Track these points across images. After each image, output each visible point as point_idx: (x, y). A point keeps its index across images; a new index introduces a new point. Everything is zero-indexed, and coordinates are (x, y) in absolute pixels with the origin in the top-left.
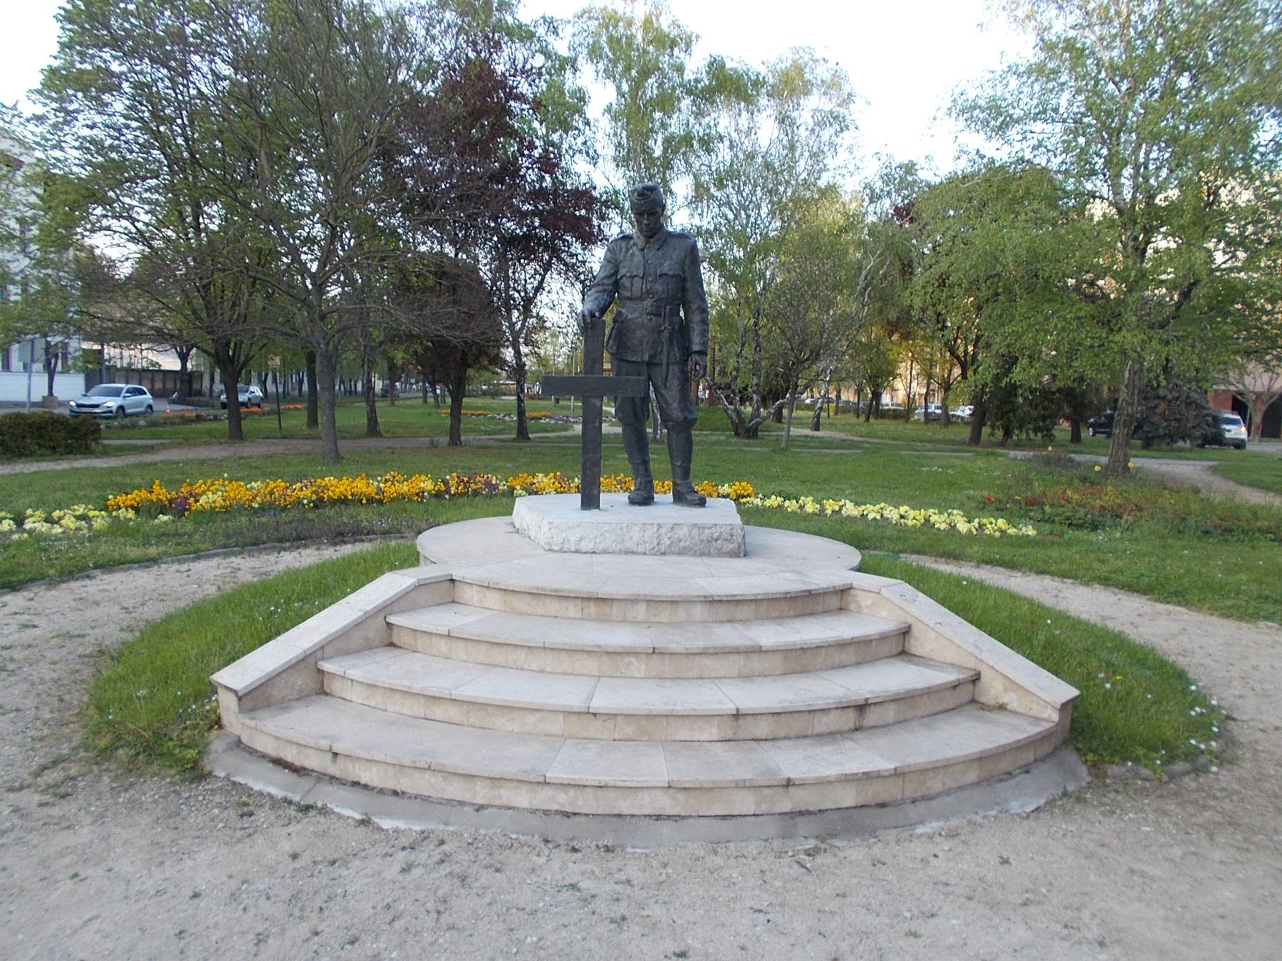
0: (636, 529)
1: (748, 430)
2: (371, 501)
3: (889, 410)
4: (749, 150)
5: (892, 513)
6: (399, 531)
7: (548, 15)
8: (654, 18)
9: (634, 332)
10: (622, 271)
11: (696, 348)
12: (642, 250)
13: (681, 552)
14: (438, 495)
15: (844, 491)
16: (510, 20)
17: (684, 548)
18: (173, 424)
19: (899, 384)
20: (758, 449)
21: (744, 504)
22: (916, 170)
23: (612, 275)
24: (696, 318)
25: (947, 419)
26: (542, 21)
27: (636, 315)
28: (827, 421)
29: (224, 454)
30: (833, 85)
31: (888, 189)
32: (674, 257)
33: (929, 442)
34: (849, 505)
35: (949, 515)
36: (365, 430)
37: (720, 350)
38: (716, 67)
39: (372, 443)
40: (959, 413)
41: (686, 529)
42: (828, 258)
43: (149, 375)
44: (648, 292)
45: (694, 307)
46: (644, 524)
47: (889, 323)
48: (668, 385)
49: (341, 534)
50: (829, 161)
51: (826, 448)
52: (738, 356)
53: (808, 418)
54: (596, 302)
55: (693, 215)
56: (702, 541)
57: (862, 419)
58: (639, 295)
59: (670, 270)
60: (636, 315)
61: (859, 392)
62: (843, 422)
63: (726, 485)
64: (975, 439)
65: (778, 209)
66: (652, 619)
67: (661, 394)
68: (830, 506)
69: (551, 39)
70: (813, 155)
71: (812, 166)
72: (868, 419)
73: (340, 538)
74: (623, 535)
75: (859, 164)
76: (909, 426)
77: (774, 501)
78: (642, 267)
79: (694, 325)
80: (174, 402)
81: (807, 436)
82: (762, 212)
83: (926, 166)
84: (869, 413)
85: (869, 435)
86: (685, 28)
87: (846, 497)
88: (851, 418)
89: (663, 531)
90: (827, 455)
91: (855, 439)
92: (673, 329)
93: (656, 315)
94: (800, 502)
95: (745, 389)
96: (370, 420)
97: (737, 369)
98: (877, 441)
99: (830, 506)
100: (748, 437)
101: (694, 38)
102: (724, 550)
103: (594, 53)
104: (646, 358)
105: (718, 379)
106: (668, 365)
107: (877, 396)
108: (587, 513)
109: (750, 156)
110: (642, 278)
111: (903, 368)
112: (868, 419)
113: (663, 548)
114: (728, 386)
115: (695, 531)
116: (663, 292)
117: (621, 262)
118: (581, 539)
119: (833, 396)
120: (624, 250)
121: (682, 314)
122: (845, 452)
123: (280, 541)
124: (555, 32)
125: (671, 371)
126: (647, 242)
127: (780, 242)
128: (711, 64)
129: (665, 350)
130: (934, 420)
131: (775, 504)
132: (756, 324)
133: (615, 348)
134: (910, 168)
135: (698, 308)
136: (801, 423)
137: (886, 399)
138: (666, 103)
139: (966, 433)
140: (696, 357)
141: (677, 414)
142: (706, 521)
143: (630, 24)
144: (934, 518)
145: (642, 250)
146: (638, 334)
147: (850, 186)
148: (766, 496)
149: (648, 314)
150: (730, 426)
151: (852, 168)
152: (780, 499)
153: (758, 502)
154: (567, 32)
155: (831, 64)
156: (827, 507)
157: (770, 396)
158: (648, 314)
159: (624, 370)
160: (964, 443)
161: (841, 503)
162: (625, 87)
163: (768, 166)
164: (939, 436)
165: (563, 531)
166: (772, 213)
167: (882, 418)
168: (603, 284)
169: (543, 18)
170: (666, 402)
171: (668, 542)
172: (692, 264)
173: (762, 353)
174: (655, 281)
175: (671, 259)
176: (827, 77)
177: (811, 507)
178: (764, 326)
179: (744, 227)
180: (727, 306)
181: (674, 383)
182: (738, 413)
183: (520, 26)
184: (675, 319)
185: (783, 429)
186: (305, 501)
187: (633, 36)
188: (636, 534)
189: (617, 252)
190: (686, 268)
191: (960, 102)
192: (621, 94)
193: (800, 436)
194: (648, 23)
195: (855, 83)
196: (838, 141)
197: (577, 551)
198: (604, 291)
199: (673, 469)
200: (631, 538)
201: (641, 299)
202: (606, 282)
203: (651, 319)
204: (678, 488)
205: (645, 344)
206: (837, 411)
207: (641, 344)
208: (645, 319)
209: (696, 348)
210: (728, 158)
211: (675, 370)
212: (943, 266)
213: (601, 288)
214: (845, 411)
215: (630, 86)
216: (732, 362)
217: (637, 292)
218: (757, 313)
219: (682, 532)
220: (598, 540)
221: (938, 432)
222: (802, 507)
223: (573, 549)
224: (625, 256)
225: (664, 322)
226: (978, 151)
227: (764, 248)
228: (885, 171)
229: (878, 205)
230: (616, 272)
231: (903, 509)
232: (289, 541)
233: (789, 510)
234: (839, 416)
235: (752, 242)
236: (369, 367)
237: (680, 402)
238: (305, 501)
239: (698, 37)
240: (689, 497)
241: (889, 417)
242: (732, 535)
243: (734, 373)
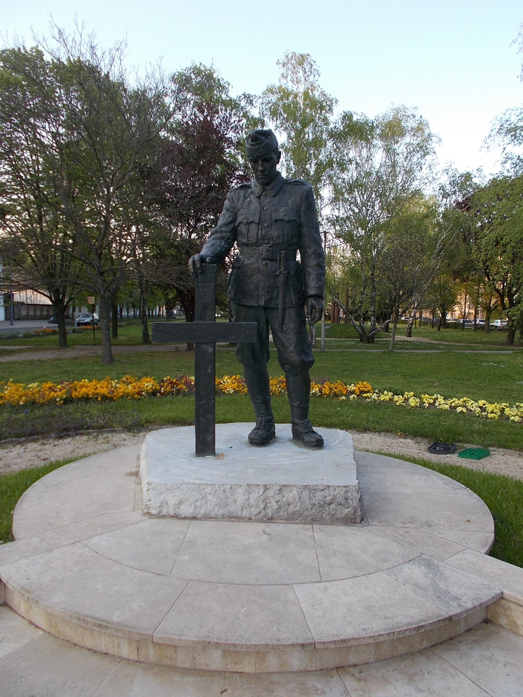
0: (241, 491)
1: (368, 338)
2: (105, 398)
3: (451, 323)
4: (368, 171)
5: (474, 406)
6: (111, 426)
7: (247, 92)
8: (310, 91)
9: (251, 276)
10: (240, 219)
11: (312, 292)
12: (259, 197)
13: (291, 518)
14: (154, 393)
15: (433, 383)
16: (224, 96)
17: (293, 513)
18: (38, 336)
19: (456, 308)
20: (374, 351)
21: (366, 398)
22: (472, 178)
23: (230, 223)
24: (312, 262)
25: (488, 329)
26: (243, 97)
27: (252, 260)
28: (415, 330)
29: (52, 356)
30: (419, 129)
31: (454, 190)
32: (290, 202)
33: (480, 343)
34: (441, 400)
35: (517, 407)
36: (141, 340)
37: (352, 291)
38: (347, 117)
39: (145, 348)
40: (494, 324)
41: (295, 491)
42: (417, 233)
43: (40, 307)
44: (263, 237)
45: (310, 251)
46: (249, 485)
47: (454, 272)
48: (285, 329)
49: (67, 430)
50: (418, 174)
51: (416, 349)
52: (362, 293)
53: (405, 328)
54: (212, 248)
55: (334, 209)
56: (313, 505)
57: (436, 329)
58: (255, 241)
59: (285, 216)
60: (252, 260)
61: (433, 313)
62: (425, 331)
63: (353, 385)
64: (511, 341)
65: (387, 207)
66: (231, 667)
67: (278, 337)
68: (427, 399)
69: (249, 108)
70: (407, 172)
71: (406, 178)
72: (439, 329)
73: (65, 433)
74: (227, 497)
75: (435, 177)
76: (465, 333)
77: (386, 396)
78: (258, 214)
79: (310, 270)
80: (52, 322)
81: (404, 341)
82: (375, 208)
83: (478, 175)
84: (441, 325)
85: (441, 339)
86: (329, 96)
87: (437, 393)
88: (428, 328)
89: (270, 493)
90: (418, 354)
91: (434, 342)
92: (289, 273)
93: (271, 260)
94: (405, 396)
95: (366, 312)
96: (144, 334)
97: (361, 302)
98: (447, 343)
99: (427, 399)
100: (369, 343)
101: (334, 101)
102: (338, 515)
103: (274, 114)
104: (262, 303)
105: (350, 307)
106: (284, 309)
107: (444, 315)
108: (201, 461)
109: (369, 174)
110: (258, 224)
111: (461, 298)
112: (439, 329)
113: (270, 512)
114: (356, 312)
115: (306, 494)
116: (278, 237)
117: (239, 210)
118: (181, 502)
119: (418, 315)
120: (242, 198)
121: (298, 258)
122: (430, 351)
123: (18, 436)
124: (251, 103)
125: (287, 315)
126: (264, 190)
127: (387, 225)
128: (344, 118)
129: (281, 295)
130: (479, 328)
131: (387, 398)
132: (372, 274)
133: (232, 293)
134: (468, 176)
135: (314, 253)
136: (401, 333)
137: (448, 317)
138: (318, 143)
139: (504, 336)
140: (311, 301)
141: (294, 358)
142: (319, 483)
143: (296, 96)
144: (507, 411)
145: (259, 197)
146: (255, 279)
147: (429, 191)
148: (381, 392)
149: (264, 259)
150: (357, 335)
151: (430, 179)
152: (390, 394)
153: (374, 396)
154: (257, 103)
155: (418, 117)
156: (425, 400)
157: (382, 317)
158: (264, 259)
159: (243, 314)
160: (503, 344)
161: (434, 397)
162: (293, 134)
163: (379, 178)
164: (485, 340)
165: (161, 494)
166: (382, 208)
167: (448, 328)
168: (221, 231)
169: (244, 94)
170: (283, 345)
171: (276, 506)
172: (308, 210)
173: (377, 292)
174: (270, 226)
175: (287, 205)
176: (415, 125)
177: (413, 402)
178: (378, 276)
179: (365, 218)
180: (355, 264)
181: (291, 326)
182: (362, 328)
183: (231, 100)
184: (292, 264)
185: (390, 337)
186: (58, 399)
187: (297, 103)
188: (240, 496)
189: (235, 200)
190: (302, 214)
191: (505, 126)
192: (289, 137)
193: (400, 341)
194: (306, 94)
195: (433, 128)
196: (423, 161)
197: (176, 517)
198: (222, 238)
199: (292, 408)
200: (235, 502)
201: (257, 244)
202: (224, 229)
203: (266, 264)
204: (296, 428)
205: (260, 289)
206: (421, 324)
207: (257, 288)
208: (261, 264)
209: (312, 292)
210: (355, 174)
211: (291, 313)
212: (499, 230)
213: (218, 235)
214: (425, 324)
215: (296, 134)
216: (358, 298)
217: (253, 239)
218: (373, 267)
219: (291, 495)
220: (199, 504)
221: (486, 337)
222: (406, 400)
223: (172, 513)
224: (242, 204)
225: (280, 268)
226: (519, 157)
227: (377, 228)
228: (452, 179)
229: (448, 200)
230: (234, 220)
231: (481, 402)
232: (24, 436)
233: (398, 404)
234: (422, 327)
235: (369, 226)
236: (143, 303)
237: (296, 346)
238: (58, 399)
239: (337, 101)
240: (306, 438)
241: (451, 327)
242: (347, 499)
243: (360, 304)
